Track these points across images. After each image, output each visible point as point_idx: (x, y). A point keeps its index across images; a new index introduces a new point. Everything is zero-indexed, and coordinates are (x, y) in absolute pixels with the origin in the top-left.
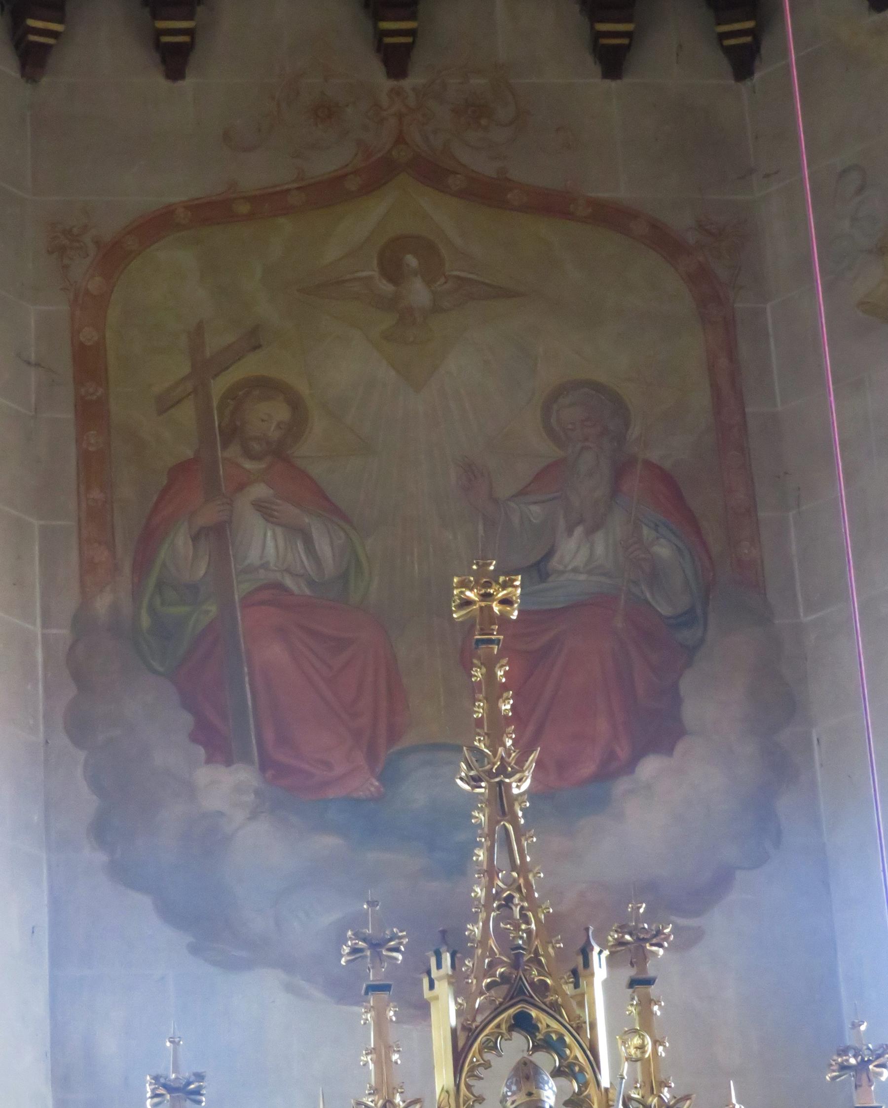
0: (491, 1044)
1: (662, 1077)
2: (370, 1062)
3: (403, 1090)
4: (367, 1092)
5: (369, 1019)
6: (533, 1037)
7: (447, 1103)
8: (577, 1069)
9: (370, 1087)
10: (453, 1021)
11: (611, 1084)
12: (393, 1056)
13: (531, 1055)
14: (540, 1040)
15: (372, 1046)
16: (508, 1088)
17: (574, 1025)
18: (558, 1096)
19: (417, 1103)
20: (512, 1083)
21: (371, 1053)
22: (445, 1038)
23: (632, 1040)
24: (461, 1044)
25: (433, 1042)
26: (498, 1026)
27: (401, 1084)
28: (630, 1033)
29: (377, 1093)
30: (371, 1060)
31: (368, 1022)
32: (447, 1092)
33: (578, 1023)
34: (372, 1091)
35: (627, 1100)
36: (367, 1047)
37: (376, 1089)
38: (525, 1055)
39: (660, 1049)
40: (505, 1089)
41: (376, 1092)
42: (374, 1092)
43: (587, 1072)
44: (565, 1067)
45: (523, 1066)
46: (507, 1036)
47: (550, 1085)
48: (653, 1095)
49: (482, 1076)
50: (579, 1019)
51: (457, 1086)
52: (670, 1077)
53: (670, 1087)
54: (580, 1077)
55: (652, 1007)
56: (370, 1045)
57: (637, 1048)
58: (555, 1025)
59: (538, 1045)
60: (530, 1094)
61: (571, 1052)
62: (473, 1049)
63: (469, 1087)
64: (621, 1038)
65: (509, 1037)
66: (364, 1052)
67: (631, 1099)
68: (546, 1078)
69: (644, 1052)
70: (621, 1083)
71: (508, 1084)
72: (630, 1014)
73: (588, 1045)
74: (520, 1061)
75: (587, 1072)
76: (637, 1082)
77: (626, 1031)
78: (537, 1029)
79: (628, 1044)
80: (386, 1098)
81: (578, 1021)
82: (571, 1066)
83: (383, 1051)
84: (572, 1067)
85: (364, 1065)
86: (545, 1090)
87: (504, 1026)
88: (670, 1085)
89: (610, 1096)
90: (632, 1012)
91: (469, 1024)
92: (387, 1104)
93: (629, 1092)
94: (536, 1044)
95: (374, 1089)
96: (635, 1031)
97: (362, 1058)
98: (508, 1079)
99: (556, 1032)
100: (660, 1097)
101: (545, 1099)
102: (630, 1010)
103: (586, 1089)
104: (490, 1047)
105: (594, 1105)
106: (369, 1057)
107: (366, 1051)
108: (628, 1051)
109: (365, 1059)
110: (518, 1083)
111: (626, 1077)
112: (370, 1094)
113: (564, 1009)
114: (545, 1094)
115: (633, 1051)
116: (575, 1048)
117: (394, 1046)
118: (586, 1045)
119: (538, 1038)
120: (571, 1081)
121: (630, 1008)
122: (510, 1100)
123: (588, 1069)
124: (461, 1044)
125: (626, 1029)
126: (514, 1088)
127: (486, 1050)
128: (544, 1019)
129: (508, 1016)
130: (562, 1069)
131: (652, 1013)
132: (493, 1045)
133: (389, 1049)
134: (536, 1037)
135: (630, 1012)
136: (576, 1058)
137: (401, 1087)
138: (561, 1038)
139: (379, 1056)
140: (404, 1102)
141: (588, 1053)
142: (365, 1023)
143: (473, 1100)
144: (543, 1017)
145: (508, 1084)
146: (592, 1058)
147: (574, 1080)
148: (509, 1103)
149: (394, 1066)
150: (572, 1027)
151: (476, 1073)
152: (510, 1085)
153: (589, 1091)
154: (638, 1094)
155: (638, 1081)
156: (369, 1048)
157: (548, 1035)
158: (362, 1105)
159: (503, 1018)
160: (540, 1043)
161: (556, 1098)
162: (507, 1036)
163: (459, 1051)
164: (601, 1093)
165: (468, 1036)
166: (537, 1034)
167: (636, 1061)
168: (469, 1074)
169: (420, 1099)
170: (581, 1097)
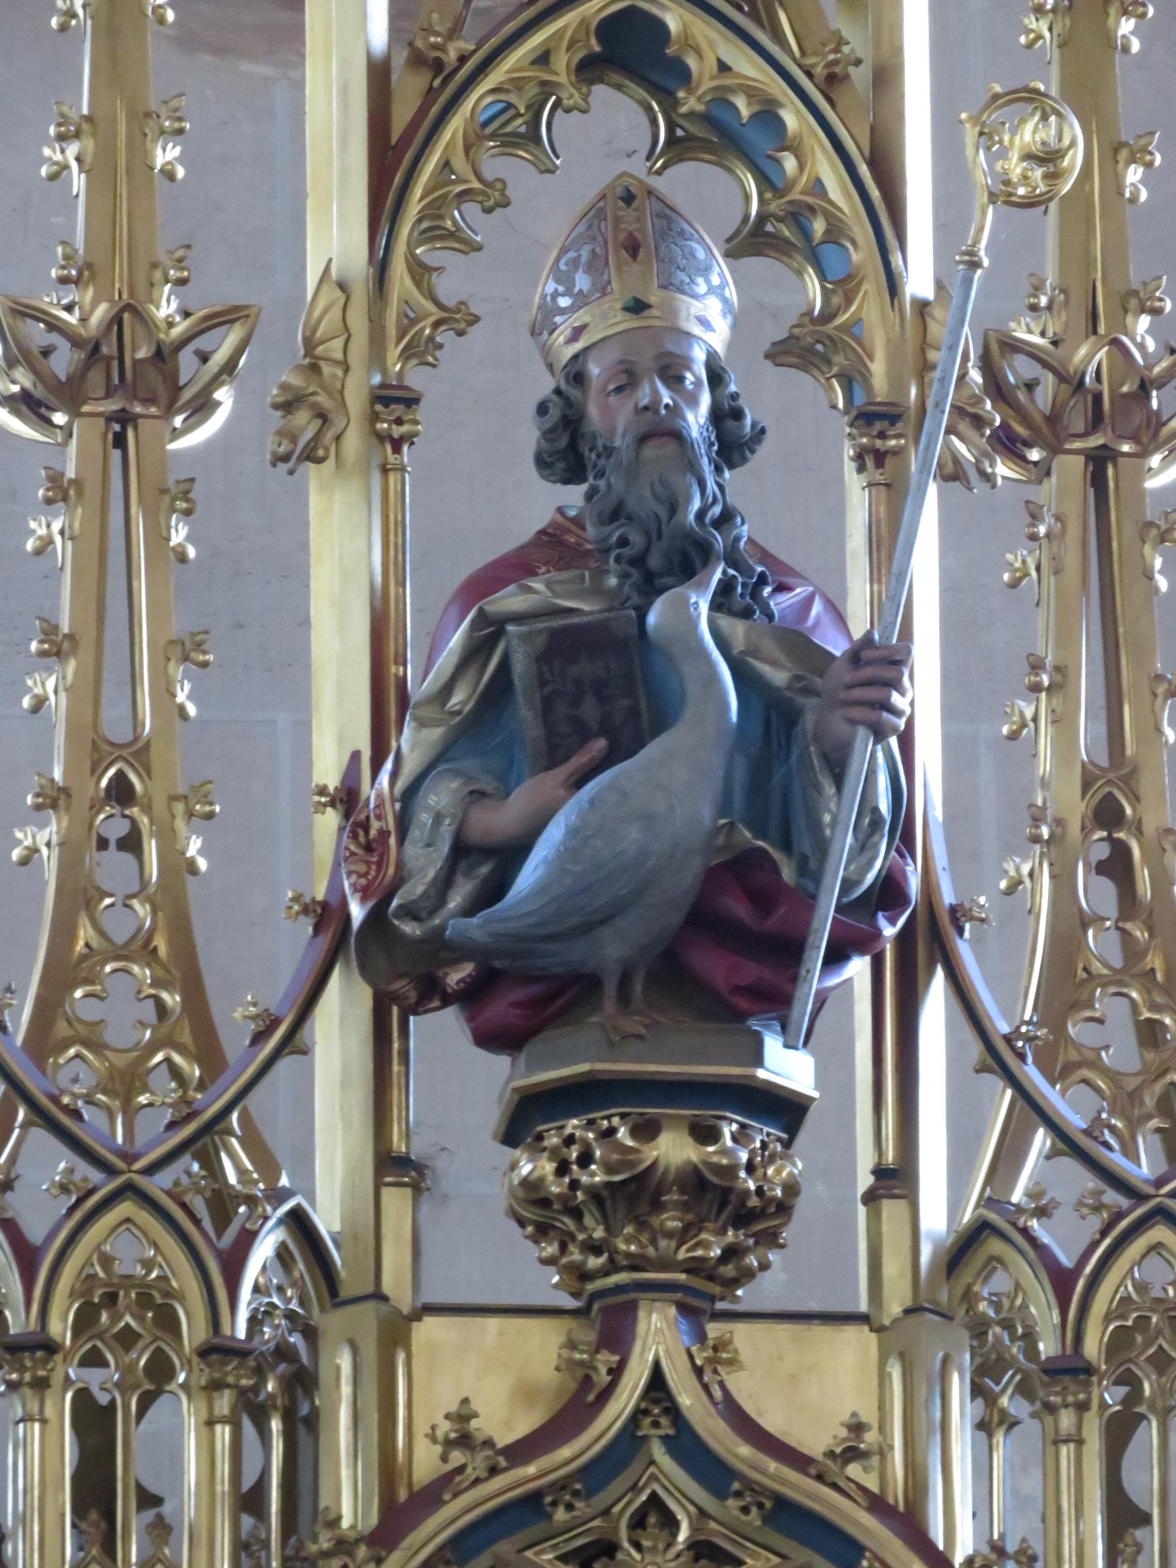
0: (519, 126)
1: (1135, 277)
2: (74, 166)
3: (186, 274)
4: (54, 273)
5: (80, 12)
6: (670, 105)
7: (341, 325)
8: (819, 227)
9: (66, 257)
10: (378, 33)
11: (940, 286)
12: (159, 151)
13: (659, 173)
14: (691, 115)
15: (85, 111)
16: (557, 281)
17: (819, 71)
18: (739, 322)
19: (232, 322)
20: (575, 263)
21: (77, 135)
22: (344, 90)
23: (1014, 131)
24: (401, 116)
25: (307, 108)
26: (543, 59)
27: (180, 253)
28: (1011, 101)
29: (93, 277)
30: (78, 159)
31: (74, 22)
32: (342, 286)
33: (835, 63)
34: (74, 272)
35: (995, 348)
36: (65, 109)
37: (89, 266)
38: (638, 167)
39: (1133, 174)
40: (551, 287)
41: (86, 273)
42: (80, 273)
43: (854, 243)
44: (780, 220)
45: (621, 204)
46: (571, 95)
47: (715, 280)
48: (1092, 339)
49: (479, 239)
50: (837, 50)
51: (381, 267)
52: (1159, 278)
53: (1156, 312)
54: (829, 253)
55: (1111, 20)
56: (80, 108)
57: (1029, 157)
58: (747, 66)
59: (689, 138)
60: (638, 307)
61: (801, 166)
62: (446, 135)
63: (420, 271)
64: (975, 119)
65: (577, 99)
66: (52, 130)
67: (1013, 347)
68: (701, 254)
69: (1053, 177)
70: (968, 282)
71: (562, 266)
72: (1030, 45)
73: (867, 153)
74: (611, 186)
75: (854, 243)
76: (1037, 289)
77: (996, 97)
78: (684, 75)
79: (1001, 142)
80: (125, 296)
81: (831, 57)
82: (798, 215)
83: (122, 128)
84: (803, 219)
85: (53, 177)
86: (695, 296)
87: (562, 62)
88: (1158, 304)
89: (934, 329)
90: (1040, 37)
91: (435, 47)
92: (126, 316)
93: (1013, 325)
94: (679, 133)
95: (80, 262)
96: (1029, 97)
97: (47, 152)
98: (564, 251)
99: (751, 92)
100: (1115, 343)
101: (697, 330)
102: (1032, 31)
103: (849, 301)
104: (514, 134)
105: (871, 359)
106: (72, 149)
107: (59, 125)
108: (999, 165)
109: (58, 157)
110: (595, 265)
111: (986, 262)
112: (64, 281)
113: (785, 9)
114: (693, 311)
115: (1015, 167)
116: (819, 154)
117: (163, 115)
118: (859, 148)
119: (684, 110)
120: (800, 273)
121: (1031, 22)
122: (565, 326)
123: (862, 230)
124: (401, 116)
125: (998, 89)
126: (582, 281)
127: (492, 144)
128: (711, 44)
129: (582, 22)
130: (769, 228)
131: (1108, 40)
132: (523, 129)
133: (142, 117)
134: (676, 103)
135: (1032, 36)
136: (818, 187)
137: (180, 260)
138: (768, 115)
139: (106, 151)
140: (187, 315)
141: (864, 170)
142: (63, 28)
143: (431, 320)
144: (706, 31)
145: (562, 266)
146: (875, 193)
147: (811, 270)
148: (560, 337)
149: (160, 182)
150: (809, 75)
151: (449, 224)
152: (568, 271)
153: (860, 308)
154: (1043, 334)
155: (1043, 281)
156: (72, 114)
157: (721, 98)
158: (39, 320)
159: (564, 29)
160: (695, 129)
161: (734, 327)
162: (571, 97)
163: (394, 139)
164: (902, 319)
165: (431, 88)
166: (681, 94)
167: (1029, 203)
168: (425, 225)
169: (237, 309)
170: (829, 328)
